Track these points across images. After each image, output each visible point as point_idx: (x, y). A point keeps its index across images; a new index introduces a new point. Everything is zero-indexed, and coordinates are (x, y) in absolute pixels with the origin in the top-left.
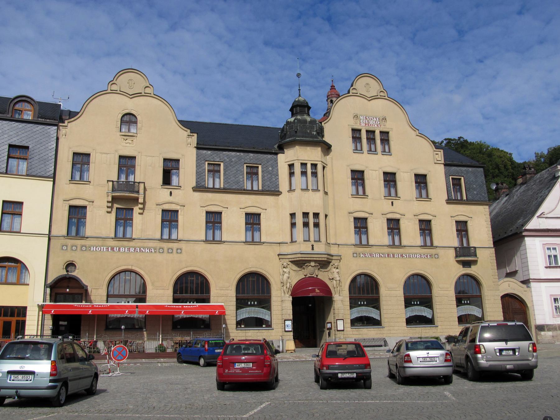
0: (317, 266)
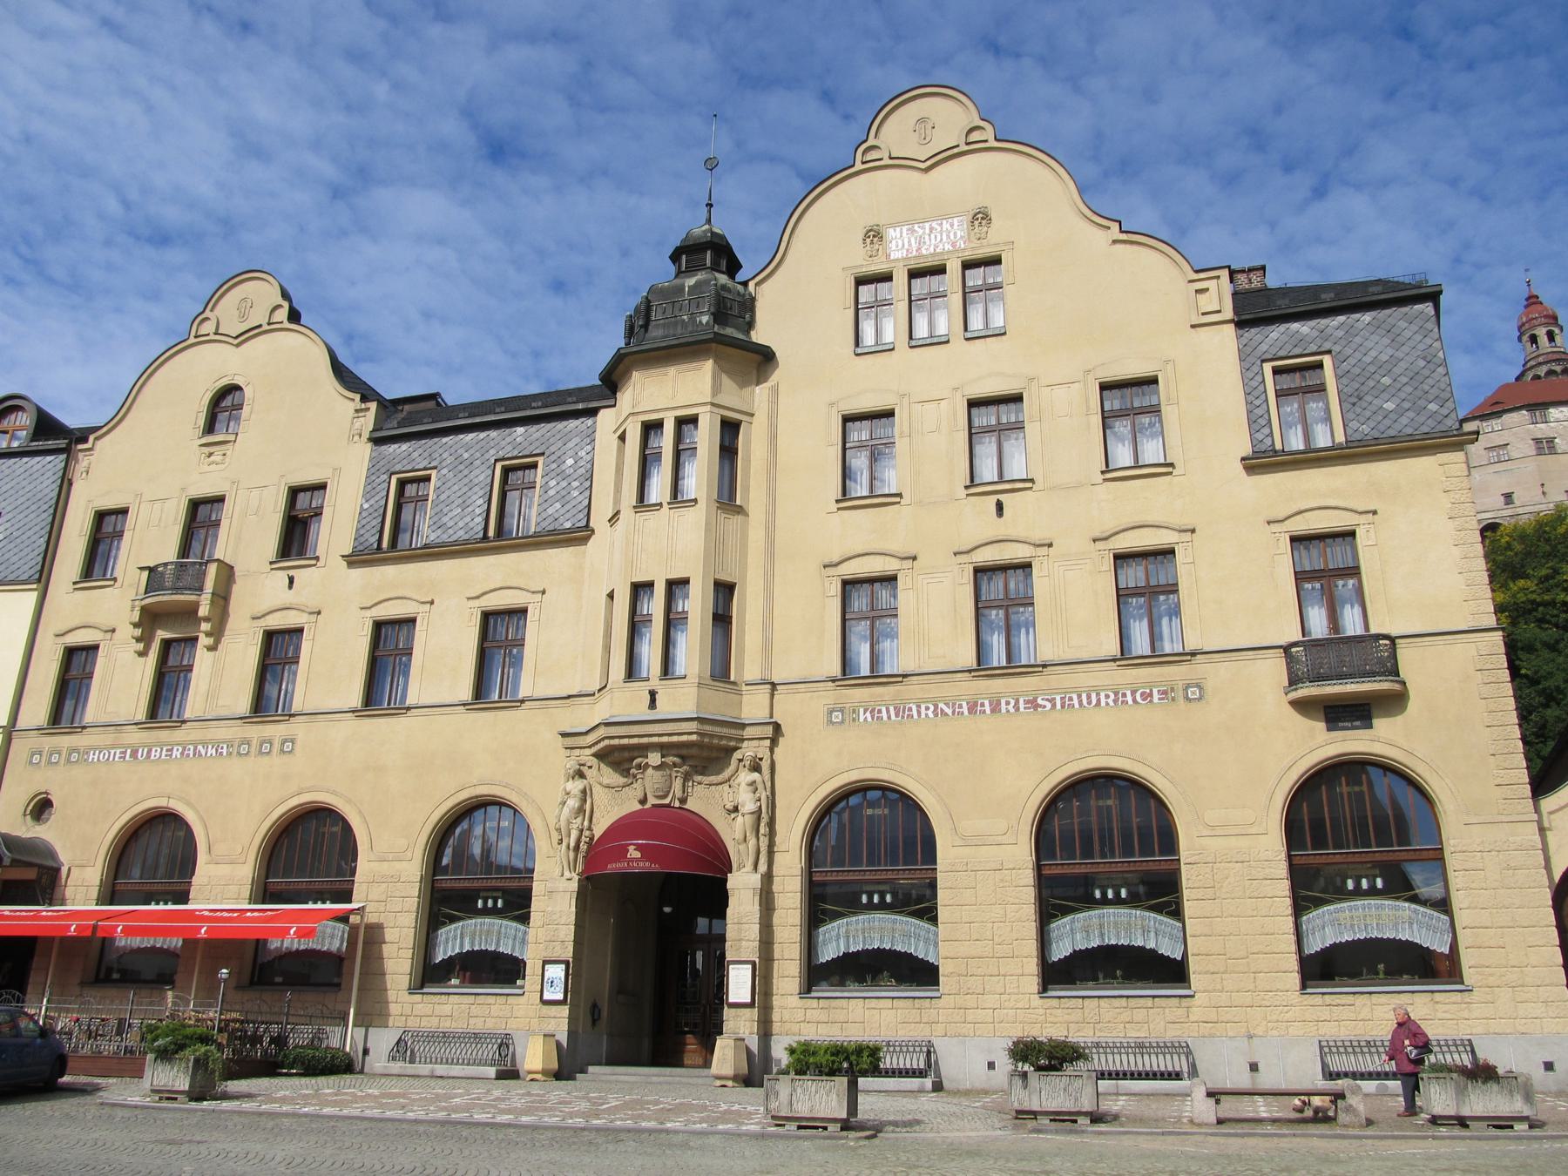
0: (675, 765)
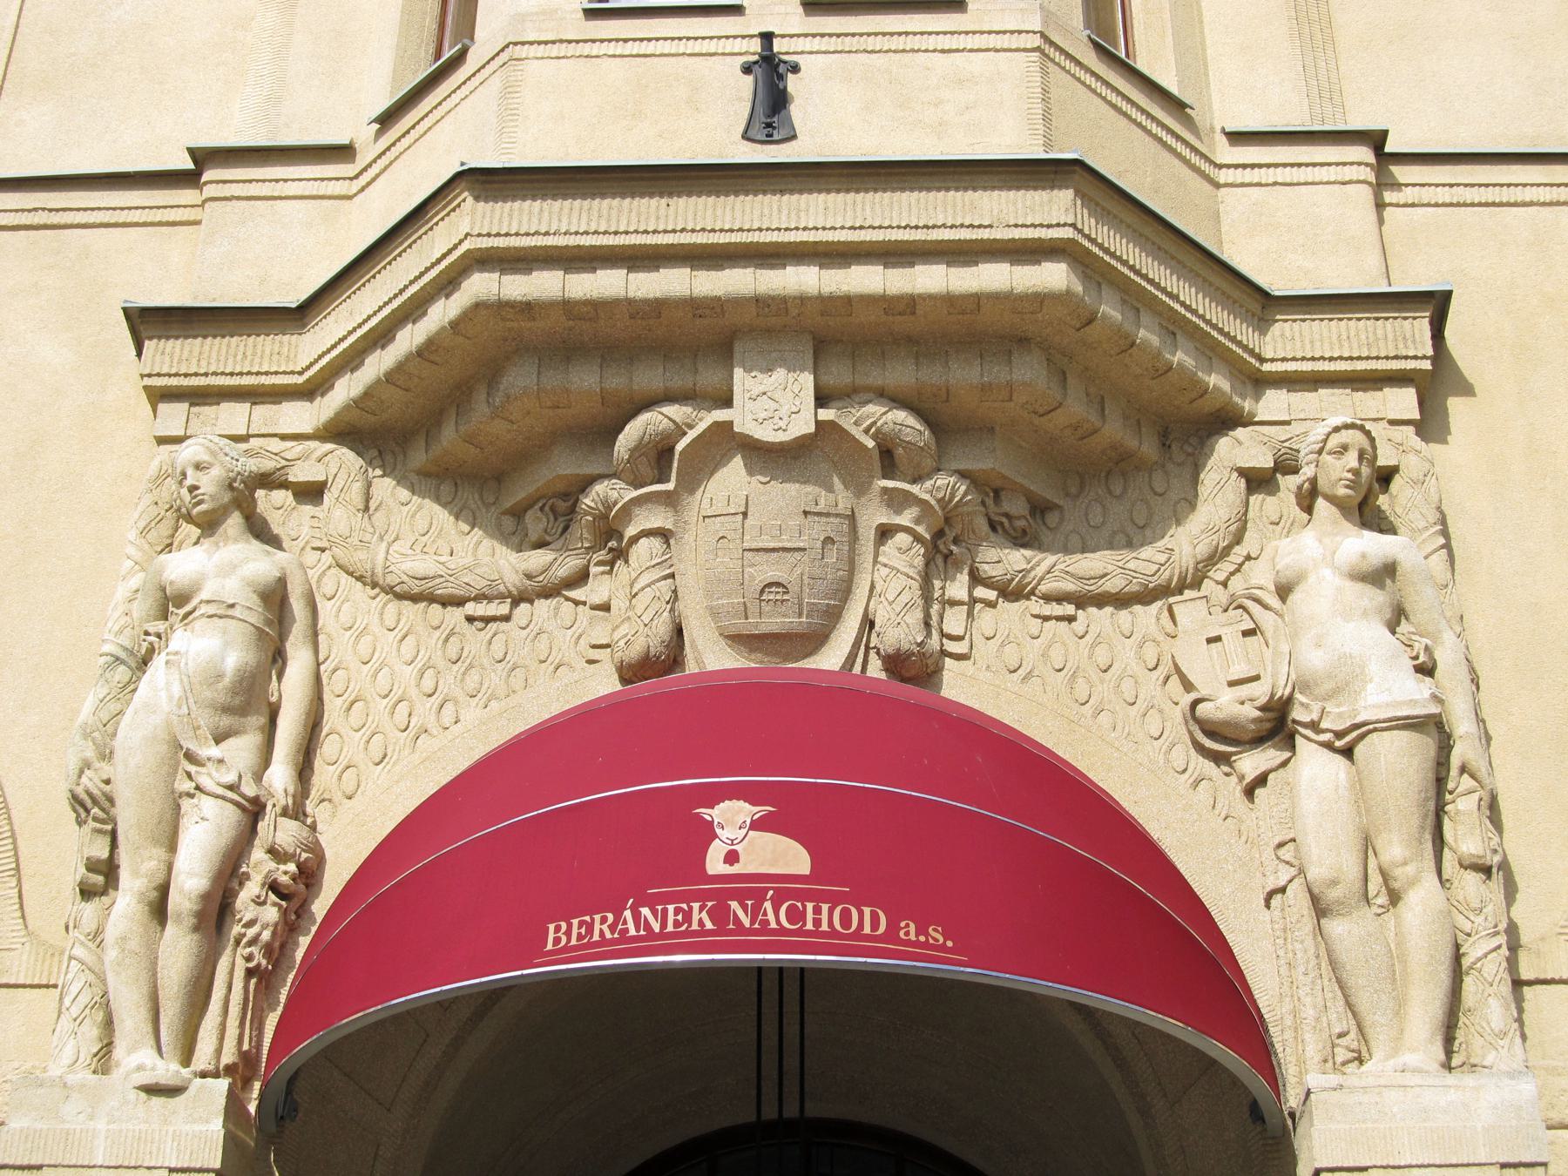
0: (888, 456)
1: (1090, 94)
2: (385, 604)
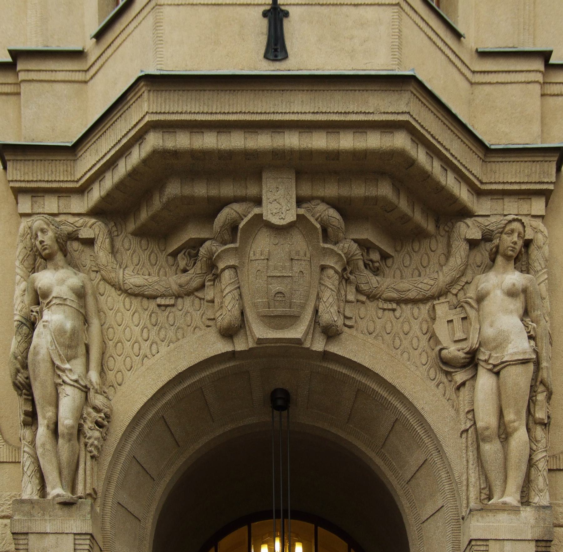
1: (420, 31)
2: (125, 299)
